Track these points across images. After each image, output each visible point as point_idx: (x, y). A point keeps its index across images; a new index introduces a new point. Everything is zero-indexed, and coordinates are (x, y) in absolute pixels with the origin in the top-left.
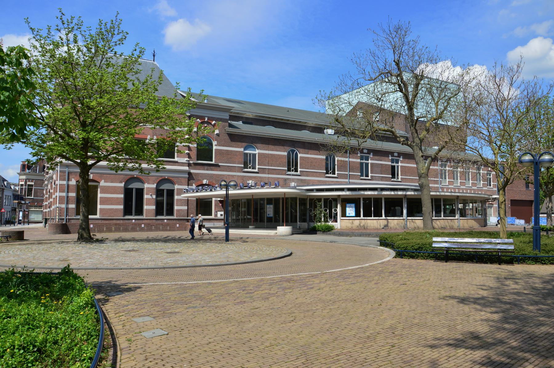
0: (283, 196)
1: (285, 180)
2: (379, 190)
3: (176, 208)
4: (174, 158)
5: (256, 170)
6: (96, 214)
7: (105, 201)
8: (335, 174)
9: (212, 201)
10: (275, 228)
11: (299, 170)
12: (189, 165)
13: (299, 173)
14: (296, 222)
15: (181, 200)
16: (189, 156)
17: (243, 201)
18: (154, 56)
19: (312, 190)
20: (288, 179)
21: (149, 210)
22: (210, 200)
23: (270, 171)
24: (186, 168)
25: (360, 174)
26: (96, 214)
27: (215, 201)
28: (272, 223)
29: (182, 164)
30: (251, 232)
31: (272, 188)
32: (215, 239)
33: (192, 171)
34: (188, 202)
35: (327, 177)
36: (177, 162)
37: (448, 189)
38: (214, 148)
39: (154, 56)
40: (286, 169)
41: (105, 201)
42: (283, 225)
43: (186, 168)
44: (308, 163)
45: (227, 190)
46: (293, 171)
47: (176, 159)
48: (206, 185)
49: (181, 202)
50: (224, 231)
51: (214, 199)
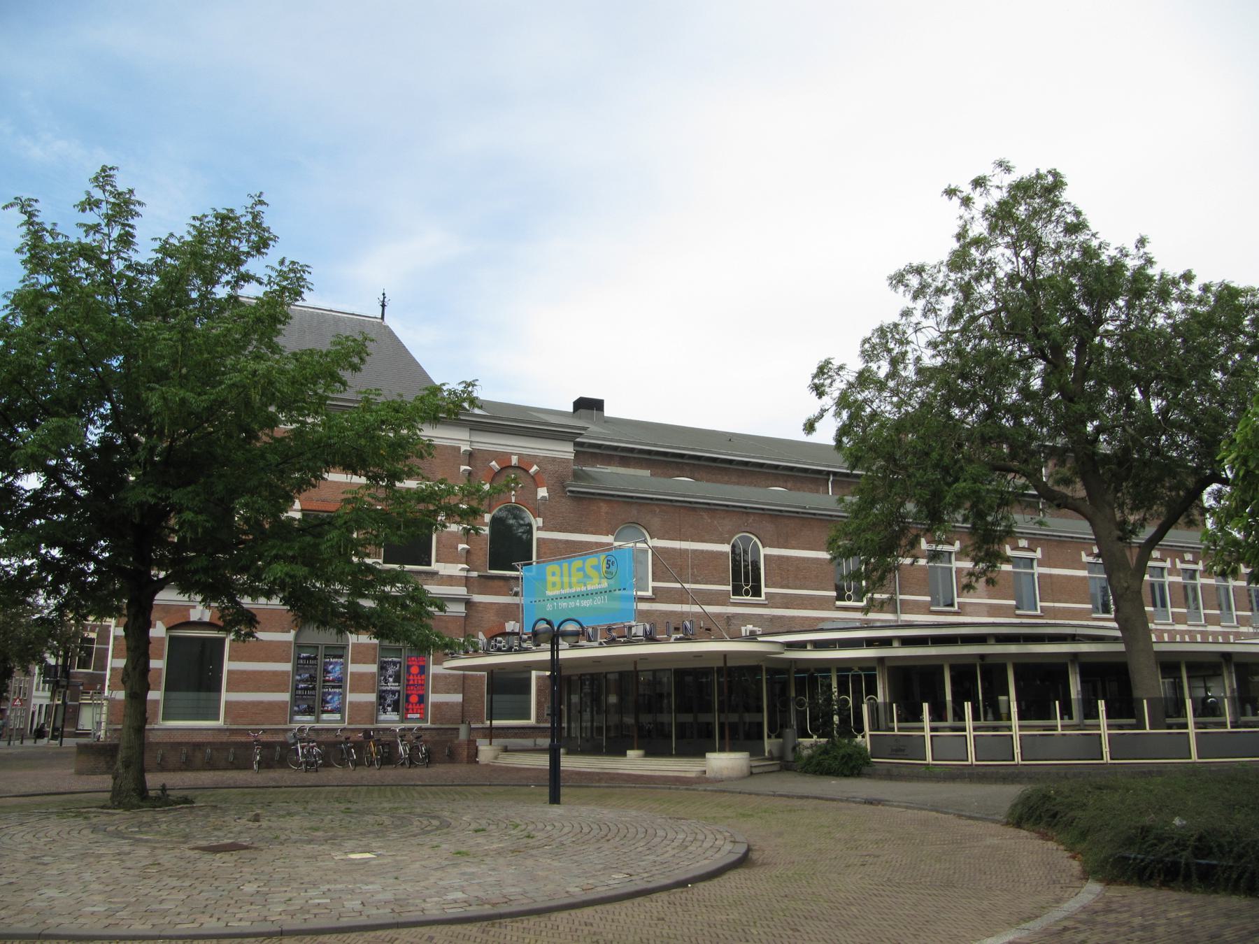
0: (721, 664)
1: (729, 618)
2: (896, 644)
3: (433, 698)
4: (430, 564)
5: (649, 593)
6: (529, 718)
7: (242, 681)
8: (952, 605)
9: (530, 679)
10: (700, 753)
11: (764, 590)
12: (467, 581)
13: (956, 608)
14: (761, 738)
15: (445, 677)
16: (468, 557)
17: (610, 677)
18: (383, 306)
19: (801, 646)
20: (735, 616)
21: (238, 703)
22: (525, 675)
23: (681, 596)
24: (461, 591)
25: (834, 594)
26: (218, 719)
27: (538, 678)
28: (696, 742)
29: (450, 581)
30: (634, 762)
31: (678, 640)
32: (512, 782)
33: (477, 598)
34: (462, 682)
35: (735, 604)
36: (435, 573)
37: (1238, 635)
38: (536, 535)
39: (383, 306)
40: (730, 588)
41: (242, 681)
42: (722, 750)
43: (461, 591)
44: (787, 572)
45: (554, 650)
46: (747, 593)
47: (435, 566)
48: (513, 633)
49: (445, 684)
50: (543, 761)
51: (534, 674)
